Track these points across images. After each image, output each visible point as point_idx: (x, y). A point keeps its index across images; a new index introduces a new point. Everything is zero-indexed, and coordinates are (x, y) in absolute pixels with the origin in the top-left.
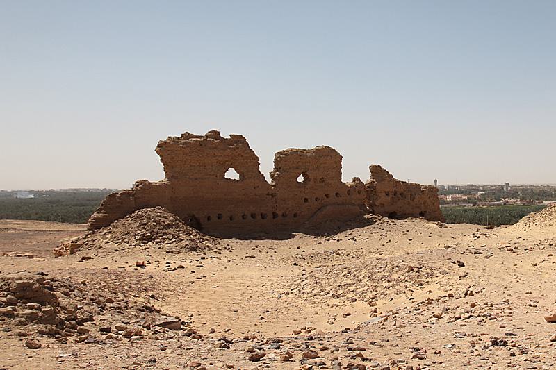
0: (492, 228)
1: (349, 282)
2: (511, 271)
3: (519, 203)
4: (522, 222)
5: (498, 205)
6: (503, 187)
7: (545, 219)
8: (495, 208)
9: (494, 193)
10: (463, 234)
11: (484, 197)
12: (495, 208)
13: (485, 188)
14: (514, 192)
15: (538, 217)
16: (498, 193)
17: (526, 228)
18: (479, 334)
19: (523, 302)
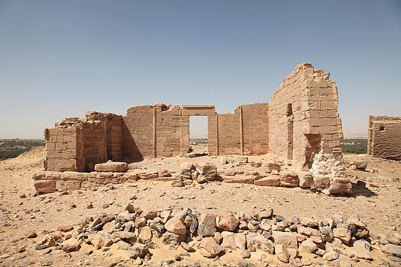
0: (3, 160)
1: (107, 181)
2: (8, 179)
3: (24, 148)
4: (19, 156)
5: (12, 149)
6: (15, 140)
7: (31, 155)
8: (10, 150)
9: (10, 143)
10: (210, 110)
11: (4, 145)
12: (10, 150)
13: (5, 141)
14: (21, 143)
15: (28, 154)
16: (12, 143)
17: (21, 159)
18: (233, 251)
19: (11, 192)
